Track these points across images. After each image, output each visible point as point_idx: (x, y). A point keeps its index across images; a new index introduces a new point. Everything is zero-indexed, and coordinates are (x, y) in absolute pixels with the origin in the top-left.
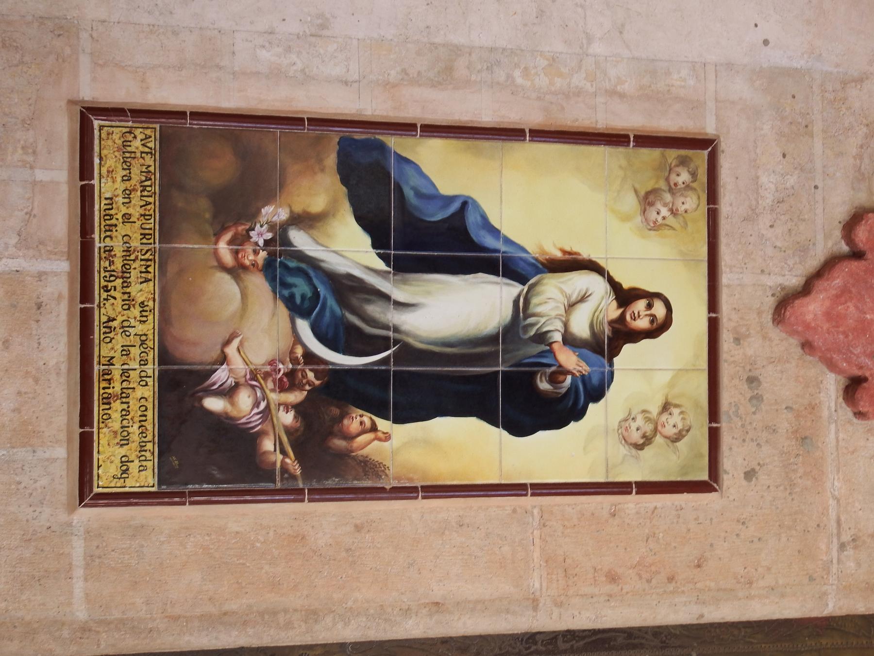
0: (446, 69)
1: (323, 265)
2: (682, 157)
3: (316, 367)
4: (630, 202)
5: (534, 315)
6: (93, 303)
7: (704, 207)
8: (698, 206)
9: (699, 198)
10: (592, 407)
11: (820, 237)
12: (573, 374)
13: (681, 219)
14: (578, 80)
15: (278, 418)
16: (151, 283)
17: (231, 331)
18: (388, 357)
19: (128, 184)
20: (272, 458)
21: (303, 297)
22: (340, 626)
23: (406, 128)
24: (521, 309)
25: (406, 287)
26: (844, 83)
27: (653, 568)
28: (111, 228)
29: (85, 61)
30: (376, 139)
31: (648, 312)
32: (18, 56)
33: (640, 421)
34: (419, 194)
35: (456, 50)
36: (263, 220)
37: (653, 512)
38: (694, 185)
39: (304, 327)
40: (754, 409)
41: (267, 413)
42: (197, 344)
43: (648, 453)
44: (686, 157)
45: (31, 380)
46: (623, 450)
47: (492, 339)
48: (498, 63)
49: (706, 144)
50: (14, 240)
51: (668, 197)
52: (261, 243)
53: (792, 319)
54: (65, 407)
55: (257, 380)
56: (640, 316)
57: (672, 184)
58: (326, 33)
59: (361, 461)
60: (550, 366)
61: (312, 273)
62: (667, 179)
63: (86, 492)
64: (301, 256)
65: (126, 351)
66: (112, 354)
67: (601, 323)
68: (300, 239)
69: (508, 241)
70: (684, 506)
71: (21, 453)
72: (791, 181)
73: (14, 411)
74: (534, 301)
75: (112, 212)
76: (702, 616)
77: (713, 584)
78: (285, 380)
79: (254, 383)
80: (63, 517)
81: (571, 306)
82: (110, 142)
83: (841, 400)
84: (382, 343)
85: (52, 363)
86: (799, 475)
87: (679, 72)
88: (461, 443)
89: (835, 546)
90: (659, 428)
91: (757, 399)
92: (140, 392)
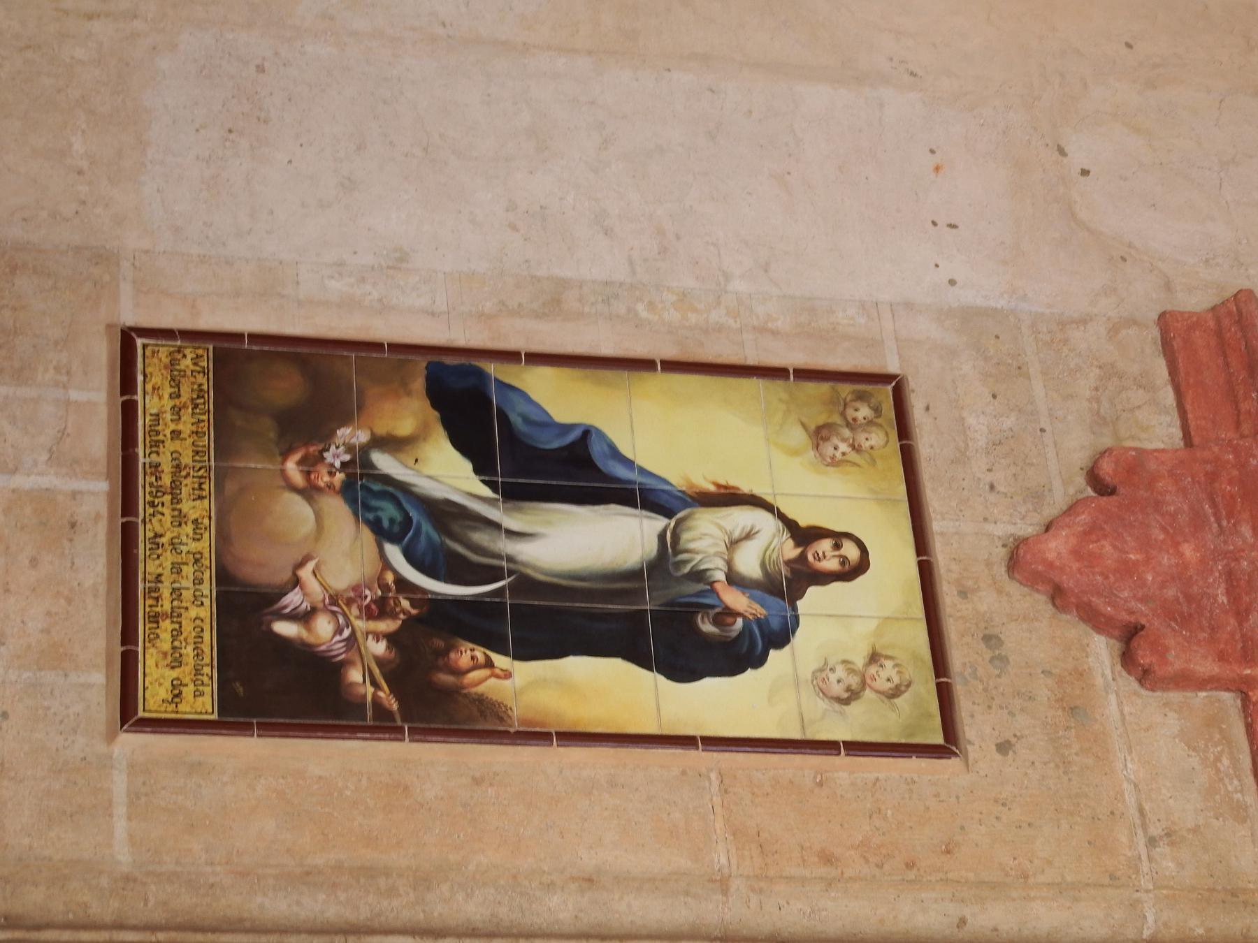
0: (554, 297)
1: (414, 489)
2: (864, 400)
3: (412, 596)
4: (798, 436)
5: (687, 551)
6: (137, 516)
7: (895, 444)
8: (887, 442)
9: (887, 434)
10: (773, 654)
11: (1057, 485)
12: (744, 617)
13: (867, 456)
14: (717, 316)
15: (366, 648)
16: (206, 501)
17: (305, 552)
18: (503, 588)
19: (177, 402)
20: (361, 690)
21: (392, 521)
22: (460, 897)
23: (511, 356)
24: (669, 547)
25: (519, 516)
26: (1063, 324)
27: (884, 851)
28: (157, 444)
29: (126, 289)
30: (471, 366)
31: (837, 553)
32: (50, 283)
33: (840, 672)
34: (527, 420)
35: (563, 284)
36: (339, 441)
37: (875, 784)
38: (879, 421)
39: (394, 553)
40: (997, 672)
41: (352, 641)
42: (262, 564)
43: (855, 708)
44: (865, 392)
45: (62, 601)
46: (822, 704)
47: (633, 575)
48: (617, 296)
50: (44, 457)
51: (847, 433)
52: (338, 464)
53: (1028, 557)
54: (104, 630)
55: (339, 606)
56: (825, 556)
57: (850, 419)
58: (404, 265)
59: (475, 700)
60: (713, 607)
61: (400, 496)
62: (843, 414)
63: (129, 713)
64: (387, 479)
65: (177, 569)
66: (160, 570)
67: (776, 563)
68: (384, 462)
69: (642, 471)
70: (916, 778)
71: (49, 677)
72: (1009, 422)
73: (42, 631)
74: (685, 536)
75: (159, 428)
76: (963, 922)
77: (971, 876)
78: (373, 607)
79: (335, 609)
80: (101, 747)
81: (733, 544)
82: (155, 360)
83: (1119, 667)
84: (492, 574)
85: (88, 583)
86: (1074, 751)
87: (844, 311)
89: (1141, 840)
90: (868, 681)
91: (1001, 661)
92: (193, 612)
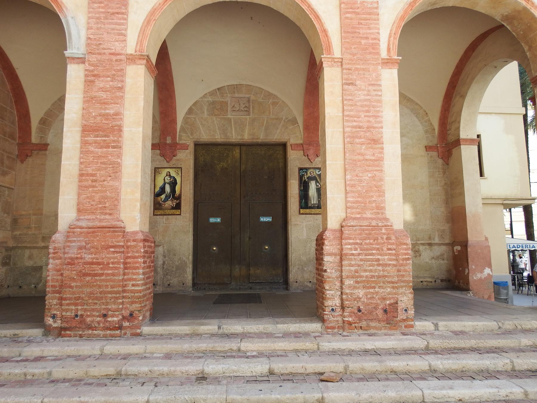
24: (168, 183)
49: (155, 168)
63: (180, 215)
88: (178, 188)
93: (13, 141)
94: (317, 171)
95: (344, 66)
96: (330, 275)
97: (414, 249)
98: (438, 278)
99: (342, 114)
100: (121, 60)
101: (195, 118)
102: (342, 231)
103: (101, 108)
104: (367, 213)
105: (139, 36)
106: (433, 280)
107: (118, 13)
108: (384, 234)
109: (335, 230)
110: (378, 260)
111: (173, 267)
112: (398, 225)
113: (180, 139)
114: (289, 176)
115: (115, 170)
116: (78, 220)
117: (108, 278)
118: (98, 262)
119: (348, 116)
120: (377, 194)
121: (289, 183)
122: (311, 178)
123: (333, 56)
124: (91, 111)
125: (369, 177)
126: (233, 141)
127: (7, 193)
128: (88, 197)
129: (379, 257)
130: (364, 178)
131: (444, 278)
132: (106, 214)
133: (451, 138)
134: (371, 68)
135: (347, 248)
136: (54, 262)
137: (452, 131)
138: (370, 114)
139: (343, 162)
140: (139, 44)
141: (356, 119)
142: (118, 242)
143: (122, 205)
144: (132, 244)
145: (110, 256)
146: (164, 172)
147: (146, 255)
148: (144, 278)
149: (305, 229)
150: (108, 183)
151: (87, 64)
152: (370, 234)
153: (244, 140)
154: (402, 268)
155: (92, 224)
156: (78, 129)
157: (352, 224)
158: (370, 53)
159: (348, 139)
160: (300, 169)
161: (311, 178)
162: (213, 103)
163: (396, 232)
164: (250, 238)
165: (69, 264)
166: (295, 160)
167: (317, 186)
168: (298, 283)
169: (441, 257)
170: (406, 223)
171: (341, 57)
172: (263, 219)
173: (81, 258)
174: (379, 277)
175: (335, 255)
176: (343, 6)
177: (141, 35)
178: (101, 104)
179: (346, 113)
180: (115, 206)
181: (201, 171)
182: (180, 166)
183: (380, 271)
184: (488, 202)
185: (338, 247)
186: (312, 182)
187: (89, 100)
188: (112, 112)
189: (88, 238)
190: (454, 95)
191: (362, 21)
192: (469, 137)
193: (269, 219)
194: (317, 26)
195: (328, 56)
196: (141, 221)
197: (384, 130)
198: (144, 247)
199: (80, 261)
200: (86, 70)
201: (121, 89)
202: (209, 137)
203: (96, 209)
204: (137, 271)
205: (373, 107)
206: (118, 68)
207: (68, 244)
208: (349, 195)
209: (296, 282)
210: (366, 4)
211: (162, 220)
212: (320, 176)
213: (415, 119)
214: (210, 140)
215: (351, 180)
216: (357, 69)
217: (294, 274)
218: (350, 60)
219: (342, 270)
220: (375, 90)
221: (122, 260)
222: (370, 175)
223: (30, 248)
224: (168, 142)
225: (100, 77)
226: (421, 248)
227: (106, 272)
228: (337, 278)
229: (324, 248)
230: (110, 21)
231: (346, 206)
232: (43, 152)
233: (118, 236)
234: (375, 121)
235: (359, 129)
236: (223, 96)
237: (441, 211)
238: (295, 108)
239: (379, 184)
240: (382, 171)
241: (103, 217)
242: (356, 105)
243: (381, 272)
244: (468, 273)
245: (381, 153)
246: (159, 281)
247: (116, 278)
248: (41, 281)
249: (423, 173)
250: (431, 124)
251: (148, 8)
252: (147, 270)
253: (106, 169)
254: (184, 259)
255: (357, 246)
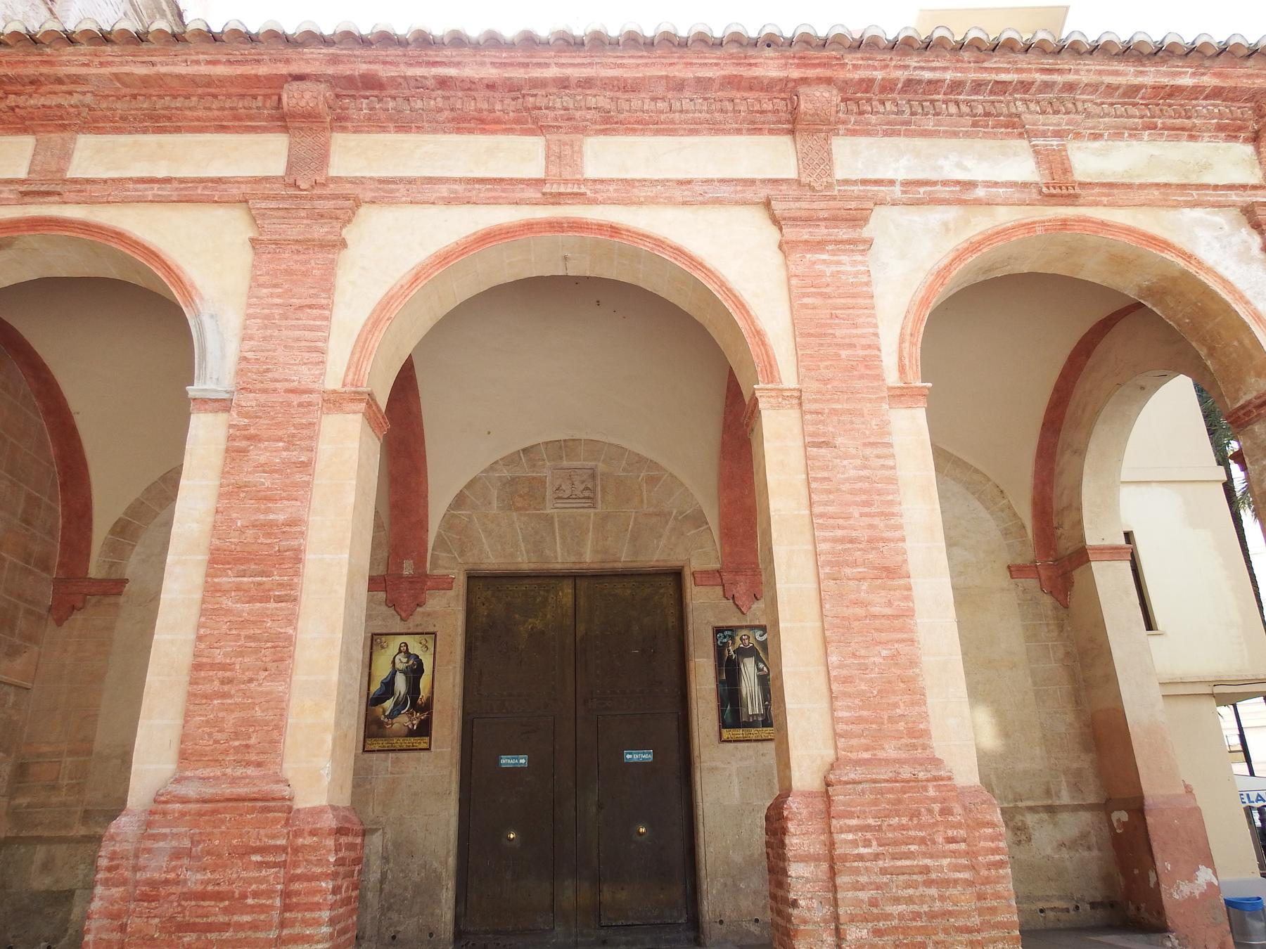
24: (401, 671)
49: (373, 635)
63: (428, 749)
88: (424, 683)
93: (45, 575)
94: (758, 633)
95: (806, 407)
96: (806, 915)
97: (1011, 824)
98: (1082, 899)
99: (808, 512)
100: (310, 404)
101: (469, 517)
102: (829, 797)
103: (258, 510)
104: (886, 746)
105: (353, 353)
106: (1071, 906)
107: (310, 307)
108: (934, 800)
109: (809, 795)
110: (926, 870)
111: (406, 889)
112: (966, 774)
113: (435, 564)
114: (691, 648)
115: (280, 652)
116: (178, 781)
117: (241, 935)
118: (219, 893)
119: (821, 516)
120: (906, 698)
121: (692, 665)
122: (744, 652)
123: (781, 386)
124: (234, 515)
125: (884, 658)
126: (559, 566)
127: (12, 699)
128: (207, 721)
129: (928, 862)
130: (872, 659)
131: (1099, 899)
132: (248, 764)
133: (1066, 546)
134: (866, 408)
135: (846, 841)
136: (107, 893)
137: (1066, 530)
138: (874, 510)
139: (819, 624)
140: (353, 369)
141: (841, 522)
142: (274, 837)
143: (289, 741)
144: (308, 841)
145: (251, 874)
146: (394, 644)
147: (341, 869)
148: (331, 935)
149: (736, 781)
150: (260, 685)
151: (234, 414)
152: (899, 801)
153: (585, 566)
154: (989, 889)
155: (211, 791)
156: (200, 557)
157: (852, 776)
158: (862, 377)
159: (827, 570)
160: (718, 630)
161: (744, 652)
162: (513, 481)
163: (962, 793)
164: (600, 807)
165: (145, 898)
166: (705, 608)
167: (759, 670)
168: (724, 926)
169: (1080, 841)
170: (982, 756)
171: (797, 386)
172: (631, 756)
173: (177, 882)
174: (932, 916)
175: (816, 859)
176: (794, 281)
177: (358, 350)
178: (258, 499)
179: (818, 510)
180: (274, 742)
181: (480, 637)
182: (431, 629)
183: (933, 899)
184: (1178, 691)
185: (822, 838)
186: (746, 660)
187: (232, 493)
188: (281, 517)
189: (197, 826)
190: (1058, 451)
191: (838, 312)
192: (1107, 543)
193: (646, 756)
194: (741, 323)
195: (770, 386)
196: (333, 780)
197: (908, 545)
198: (338, 848)
199: (173, 889)
200: (231, 426)
201: (306, 466)
202: (502, 560)
203: (225, 752)
204: (316, 914)
205: (877, 495)
206: (304, 421)
207: (148, 844)
208: (838, 704)
209: (721, 922)
210: (844, 277)
211: (383, 763)
212: (764, 645)
213: (977, 504)
214: (503, 567)
215: (841, 666)
216: (834, 412)
217: (716, 899)
218: (819, 392)
219: (836, 900)
220: (878, 457)
221: (279, 887)
222: (884, 653)
223: (50, 841)
224: (406, 573)
225: (260, 441)
226: (1030, 819)
227: (236, 918)
228: (825, 921)
229: (787, 841)
230: (294, 322)
231: (834, 730)
232: (112, 599)
233: (275, 821)
234: (886, 526)
235: (850, 546)
236: (534, 466)
237: (1065, 722)
238: (703, 493)
239: (910, 672)
240: (912, 641)
241: (239, 772)
242: (838, 490)
243: (938, 904)
244: (1158, 884)
245: (908, 598)
246: (369, 927)
247: (261, 935)
248: (66, 930)
249: (1011, 623)
250: (1015, 515)
251: (377, 294)
252: (341, 910)
253: (257, 651)
254: (435, 865)
255: (869, 835)
